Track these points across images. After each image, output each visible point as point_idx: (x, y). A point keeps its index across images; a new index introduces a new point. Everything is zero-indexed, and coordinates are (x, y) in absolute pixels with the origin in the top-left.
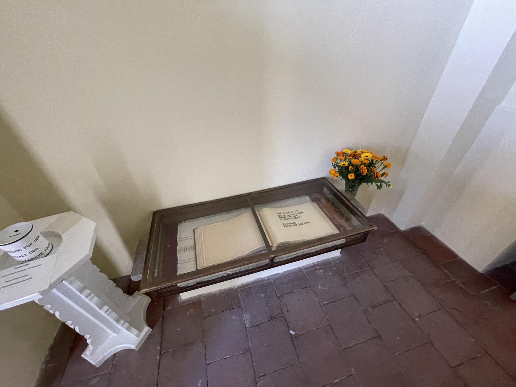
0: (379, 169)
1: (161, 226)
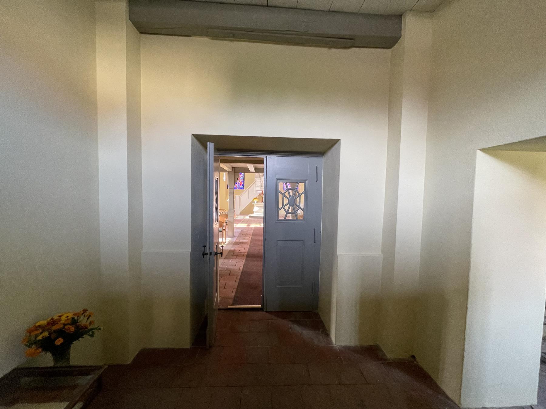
0: (83, 321)
1: (298, 204)
